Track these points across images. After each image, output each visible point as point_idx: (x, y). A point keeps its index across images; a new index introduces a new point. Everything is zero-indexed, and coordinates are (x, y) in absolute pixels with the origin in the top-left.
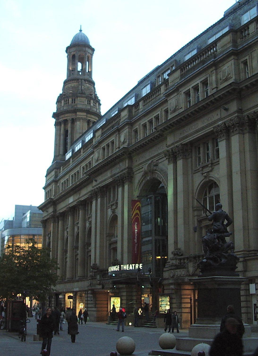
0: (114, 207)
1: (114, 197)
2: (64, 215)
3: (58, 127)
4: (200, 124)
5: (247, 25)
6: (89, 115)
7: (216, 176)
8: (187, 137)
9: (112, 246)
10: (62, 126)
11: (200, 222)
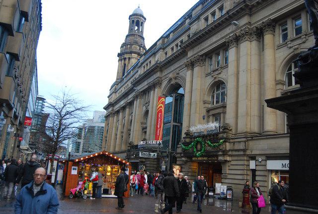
0: (147, 105)
1: (148, 98)
2: (118, 112)
3: (120, 62)
4: (214, 39)
7: (224, 77)
9: (144, 130)
10: (123, 61)
11: (208, 111)
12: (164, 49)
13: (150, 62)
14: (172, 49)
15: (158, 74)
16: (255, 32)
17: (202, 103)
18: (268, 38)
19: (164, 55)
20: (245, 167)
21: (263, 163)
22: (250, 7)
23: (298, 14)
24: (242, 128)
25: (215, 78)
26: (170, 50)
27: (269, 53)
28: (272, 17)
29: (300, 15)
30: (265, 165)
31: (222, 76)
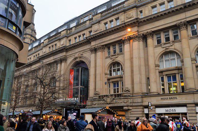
5: (72, 28)
6: (32, 37)
8: (104, 42)
11: (109, 80)
12: (68, 37)
15: (64, 54)
18: (150, 41)
20: (194, 112)
21: (154, 109)
22: (139, 22)
23: (168, 30)
24: (137, 89)
25: (114, 60)
26: (74, 39)
27: (150, 49)
28: (153, 30)
29: (169, 31)
30: (144, 111)
31: (119, 59)
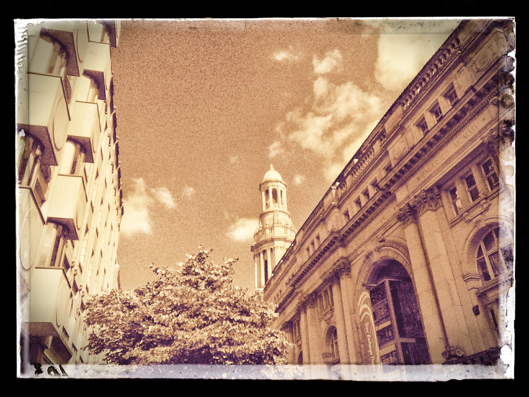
0: (328, 316)
10: (262, 255)
12: (339, 207)
13: (318, 238)
14: (358, 202)
15: (341, 252)
16: (408, 212)
17: (460, 281)
19: (343, 217)
26: (354, 205)
